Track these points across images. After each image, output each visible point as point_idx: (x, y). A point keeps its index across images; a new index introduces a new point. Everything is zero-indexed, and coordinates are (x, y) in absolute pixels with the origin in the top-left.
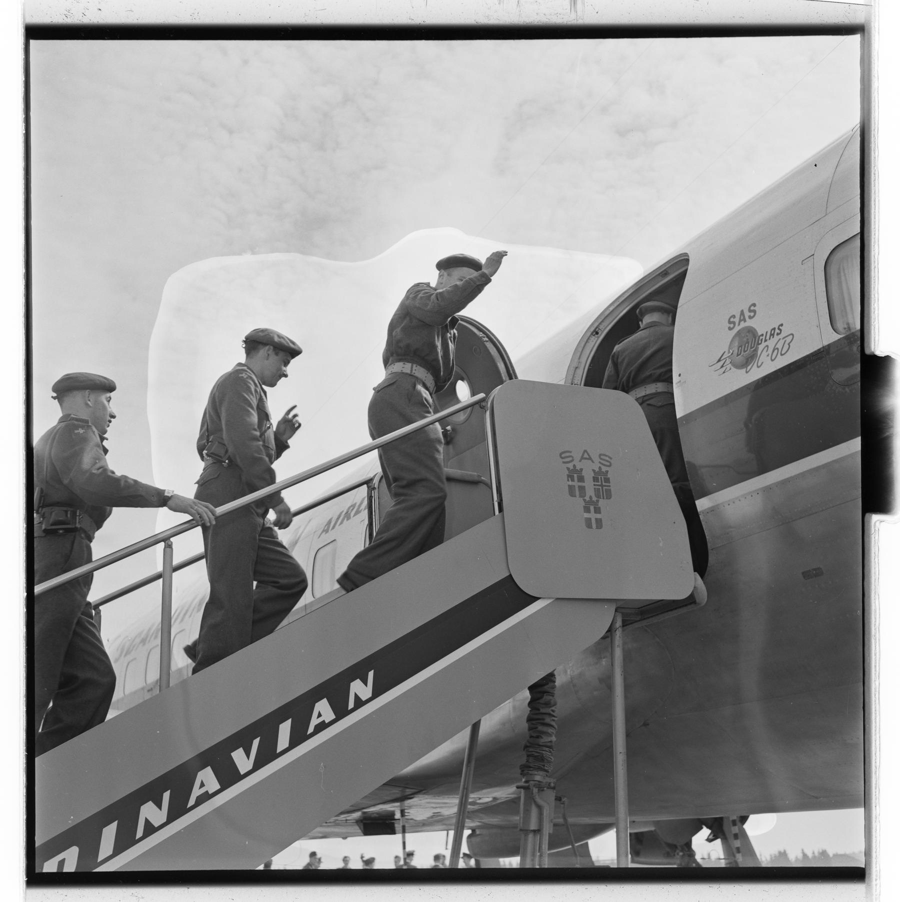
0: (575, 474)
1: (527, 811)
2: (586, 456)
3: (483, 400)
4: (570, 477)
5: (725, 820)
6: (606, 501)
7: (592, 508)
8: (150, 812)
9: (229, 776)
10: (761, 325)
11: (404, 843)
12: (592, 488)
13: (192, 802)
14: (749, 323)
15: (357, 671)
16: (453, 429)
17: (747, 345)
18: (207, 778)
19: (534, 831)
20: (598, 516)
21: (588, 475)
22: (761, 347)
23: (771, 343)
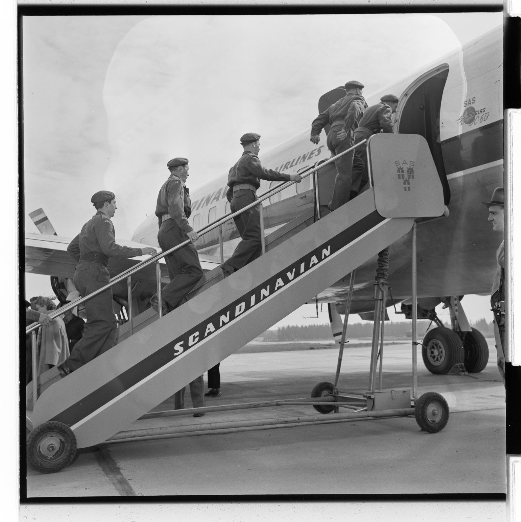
0: (400, 170)
1: (378, 293)
2: (405, 162)
3: (366, 142)
4: (399, 171)
5: (451, 299)
6: (365, 94)
7: (407, 183)
8: (264, 292)
9: (286, 281)
10: (477, 107)
12: (407, 176)
14: (472, 105)
17: (470, 114)
19: (381, 300)
20: (409, 186)
21: (405, 169)
22: (476, 116)
23: (480, 115)
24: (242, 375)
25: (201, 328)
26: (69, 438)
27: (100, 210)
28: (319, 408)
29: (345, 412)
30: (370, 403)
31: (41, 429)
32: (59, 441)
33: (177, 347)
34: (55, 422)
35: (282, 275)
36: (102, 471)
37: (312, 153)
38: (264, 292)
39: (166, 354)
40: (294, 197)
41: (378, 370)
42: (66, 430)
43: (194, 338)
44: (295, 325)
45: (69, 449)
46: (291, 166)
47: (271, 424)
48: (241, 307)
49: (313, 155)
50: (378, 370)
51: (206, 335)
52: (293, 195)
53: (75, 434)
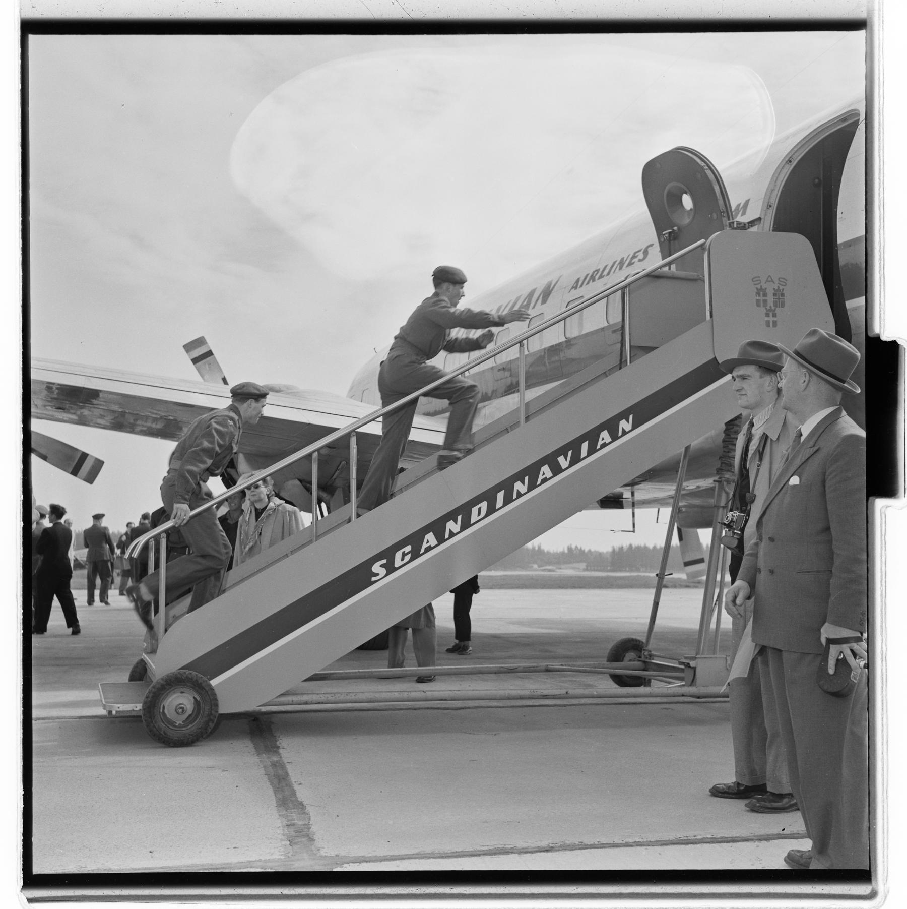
0: (761, 292)
1: (719, 495)
2: (770, 280)
3: (704, 243)
4: (758, 294)
7: (771, 314)
8: (519, 486)
9: (557, 470)
11: (634, 516)
13: (539, 482)
15: (624, 415)
16: (679, 229)
18: (546, 471)
20: (775, 319)
21: (770, 292)
24: (520, 623)
25: (415, 541)
26: (207, 696)
27: (439, 291)
28: (620, 680)
29: (658, 686)
30: (688, 674)
31: (166, 681)
32: (193, 700)
33: (377, 568)
34: (188, 672)
35: (551, 460)
36: (254, 750)
37: (634, 257)
38: (519, 486)
39: (357, 579)
40: (603, 329)
41: (713, 626)
42: (203, 685)
43: (404, 555)
44: (643, 545)
45: (206, 713)
46: (601, 277)
47: (522, 698)
48: (480, 509)
49: (636, 260)
50: (713, 626)
51: (422, 551)
52: (601, 326)
53: (217, 691)
